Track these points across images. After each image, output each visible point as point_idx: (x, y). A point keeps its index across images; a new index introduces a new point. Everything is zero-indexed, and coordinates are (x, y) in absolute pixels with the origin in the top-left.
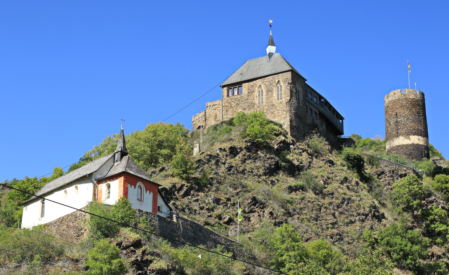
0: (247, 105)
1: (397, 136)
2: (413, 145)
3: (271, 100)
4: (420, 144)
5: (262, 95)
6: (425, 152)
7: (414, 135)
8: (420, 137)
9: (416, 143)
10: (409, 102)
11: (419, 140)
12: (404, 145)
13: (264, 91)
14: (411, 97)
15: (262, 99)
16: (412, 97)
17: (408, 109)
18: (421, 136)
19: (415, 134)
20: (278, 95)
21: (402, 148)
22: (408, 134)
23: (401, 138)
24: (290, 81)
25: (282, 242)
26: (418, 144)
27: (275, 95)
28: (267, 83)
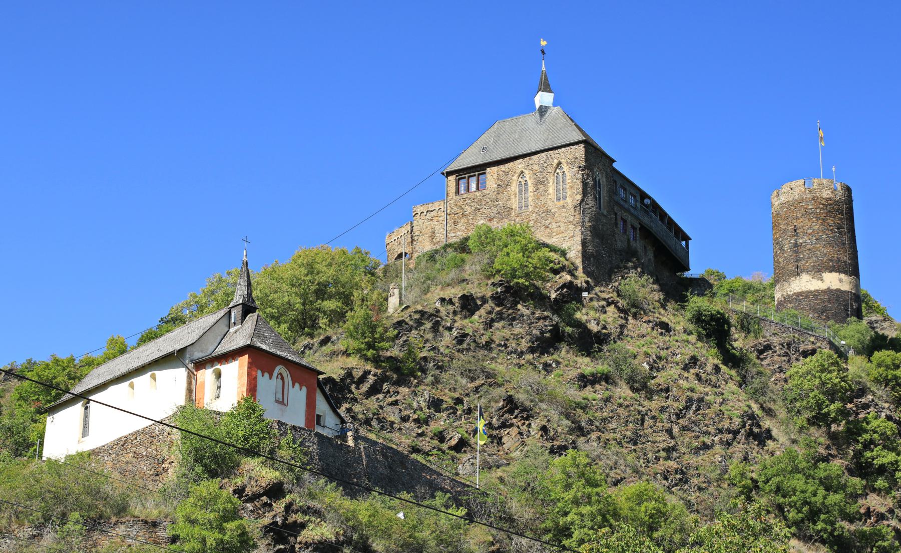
0: (495, 210)
1: (797, 273)
2: (829, 291)
3: (543, 202)
4: (842, 289)
5: (526, 190)
6: (852, 306)
7: (831, 272)
8: (843, 276)
9: (834, 287)
10: (821, 206)
11: (841, 281)
12: (811, 292)
13: (530, 183)
14: (825, 196)
15: (526, 199)
16: (826, 194)
17: (818, 219)
18: (845, 273)
19: (832, 270)
20: (558, 190)
21: (806, 297)
22: (818, 270)
23: (805, 277)
24: (583, 164)
25: (566, 486)
26: (838, 290)
27: (551, 190)
28: (535, 167)
